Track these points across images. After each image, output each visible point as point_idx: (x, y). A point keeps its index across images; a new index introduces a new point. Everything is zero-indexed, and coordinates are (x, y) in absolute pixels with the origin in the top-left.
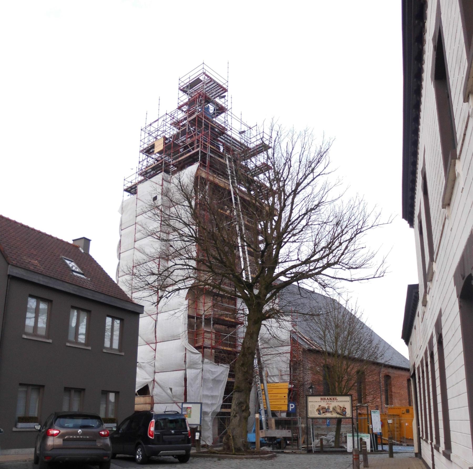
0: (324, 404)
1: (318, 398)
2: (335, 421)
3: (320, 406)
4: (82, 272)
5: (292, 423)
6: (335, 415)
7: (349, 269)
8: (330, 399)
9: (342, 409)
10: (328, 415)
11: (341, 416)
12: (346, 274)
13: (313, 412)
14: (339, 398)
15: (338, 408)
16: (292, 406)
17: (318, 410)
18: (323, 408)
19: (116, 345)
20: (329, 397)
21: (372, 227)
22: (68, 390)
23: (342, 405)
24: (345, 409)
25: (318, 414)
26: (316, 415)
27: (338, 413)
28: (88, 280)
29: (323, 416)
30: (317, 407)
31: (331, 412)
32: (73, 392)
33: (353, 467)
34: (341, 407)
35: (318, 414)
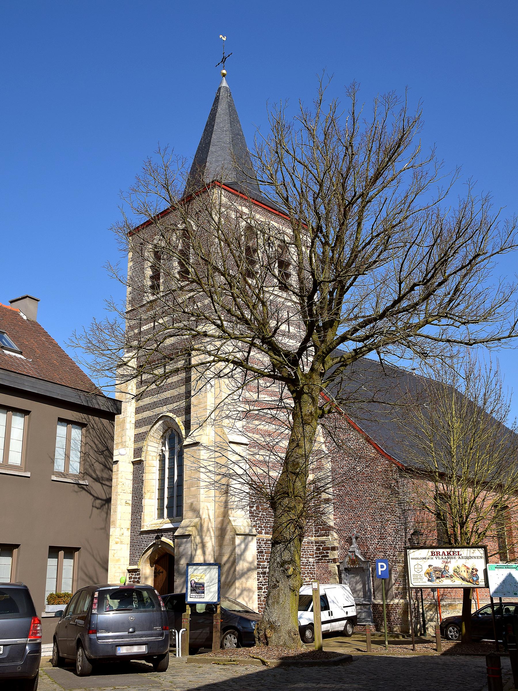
0: (438, 563)
1: (425, 553)
2: (461, 592)
3: (430, 566)
4: (19, 350)
5: (139, 459)
6: (458, 582)
7: (464, 323)
8: (449, 554)
9: (470, 571)
10: (446, 582)
11: (469, 585)
12: (460, 333)
13: (418, 578)
14: (464, 552)
15: (463, 569)
16: (382, 567)
17: (429, 574)
18: (436, 570)
19: (75, 467)
20: (446, 551)
21: (502, 250)
22: (54, 551)
23: (470, 564)
24: (477, 571)
25: (429, 580)
26: (424, 582)
27: (463, 579)
28: (28, 362)
29: (436, 583)
30: (426, 568)
31: (451, 577)
32: (61, 553)
33: (490, 689)
34: (468, 568)
35: (429, 580)
